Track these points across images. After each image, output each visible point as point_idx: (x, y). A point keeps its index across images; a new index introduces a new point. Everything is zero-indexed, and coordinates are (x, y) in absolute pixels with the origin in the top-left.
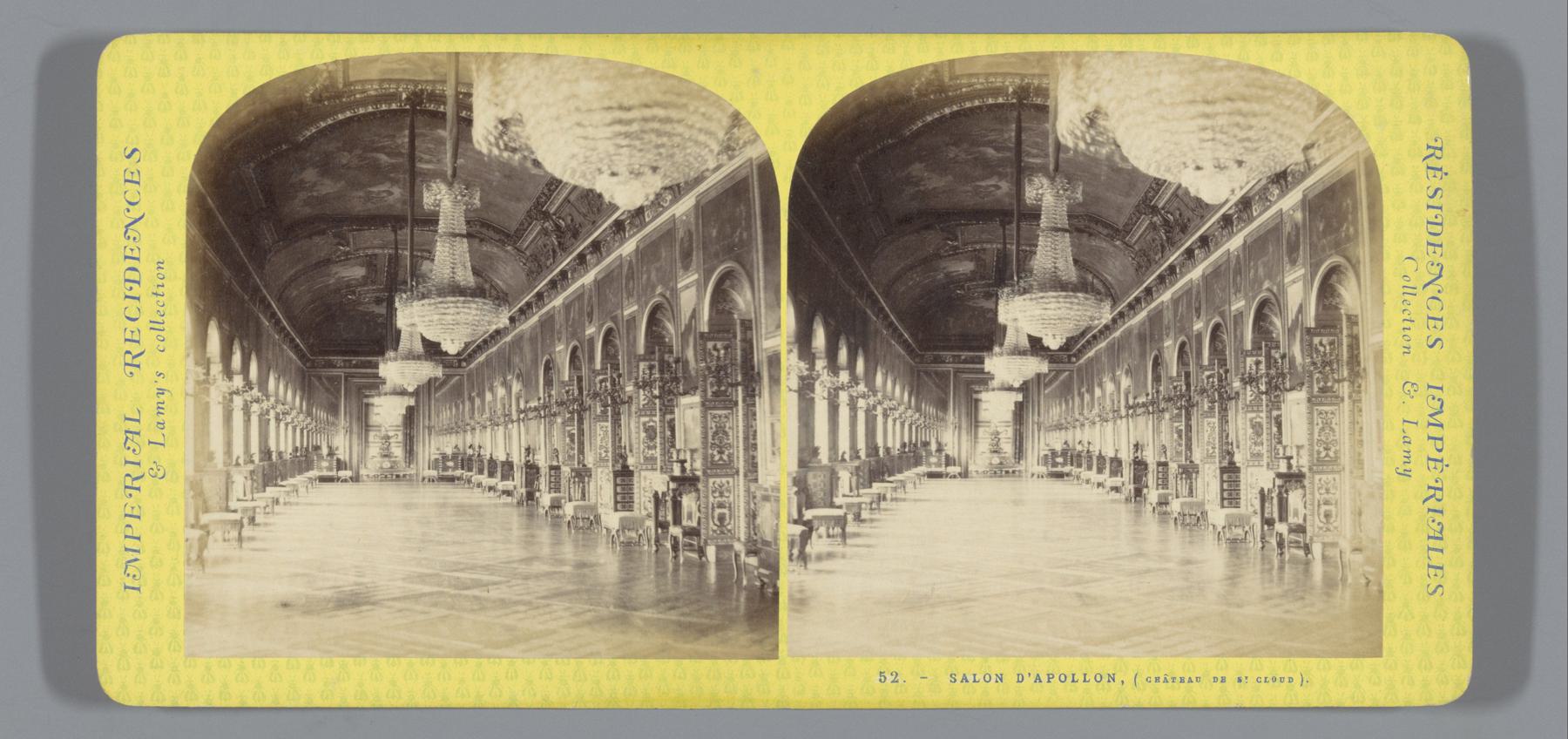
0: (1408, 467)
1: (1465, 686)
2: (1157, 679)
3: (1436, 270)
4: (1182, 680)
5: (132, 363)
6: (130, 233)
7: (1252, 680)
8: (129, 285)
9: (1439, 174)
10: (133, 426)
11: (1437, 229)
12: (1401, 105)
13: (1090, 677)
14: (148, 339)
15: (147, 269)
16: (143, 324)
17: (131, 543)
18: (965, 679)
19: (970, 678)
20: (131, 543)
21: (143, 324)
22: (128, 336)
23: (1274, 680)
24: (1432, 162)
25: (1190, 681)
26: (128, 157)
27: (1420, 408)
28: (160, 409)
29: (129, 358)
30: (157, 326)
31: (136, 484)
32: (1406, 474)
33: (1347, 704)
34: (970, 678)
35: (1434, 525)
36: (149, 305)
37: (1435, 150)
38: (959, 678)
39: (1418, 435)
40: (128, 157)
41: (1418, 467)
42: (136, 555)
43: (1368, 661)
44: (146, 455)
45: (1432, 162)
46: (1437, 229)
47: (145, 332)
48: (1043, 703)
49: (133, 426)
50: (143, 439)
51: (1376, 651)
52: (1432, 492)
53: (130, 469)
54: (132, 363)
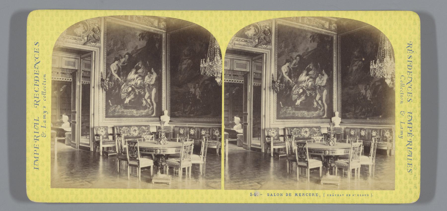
0: (402, 135)
1: (418, 198)
2: (363, 195)
3: (410, 79)
4: (338, 195)
5: (37, 103)
6: (36, 67)
7: (351, 195)
8: (35, 81)
9: (411, 52)
10: (37, 122)
11: (410, 68)
12: (41, 180)
13: (334, 195)
14: (41, 97)
15: (41, 80)
16: (40, 92)
17: (36, 156)
18: (272, 195)
19: (273, 195)
20: (36, 156)
21: (40, 92)
22: (36, 50)
23: (365, 195)
24: (409, 48)
25: (341, 195)
26: (36, 45)
27: (405, 118)
28: (44, 117)
29: (35, 138)
30: (44, 93)
31: (37, 139)
32: (401, 137)
33: (379, 203)
34: (273, 195)
35: (410, 152)
36: (41, 90)
37: (410, 45)
38: (270, 195)
39: (405, 126)
40: (36, 45)
41: (405, 134)
42: (38, 159)
43: (49, 183)
44: (41, 130)
45: (409, 48)
46: (410, 68)
47: (40, 95)
48: (301, 202)
49: (37, 122)
50: (39, 126)
51: (52, 186)
52: (409, 143)
53: (36, 134)
54: (37, 103)
